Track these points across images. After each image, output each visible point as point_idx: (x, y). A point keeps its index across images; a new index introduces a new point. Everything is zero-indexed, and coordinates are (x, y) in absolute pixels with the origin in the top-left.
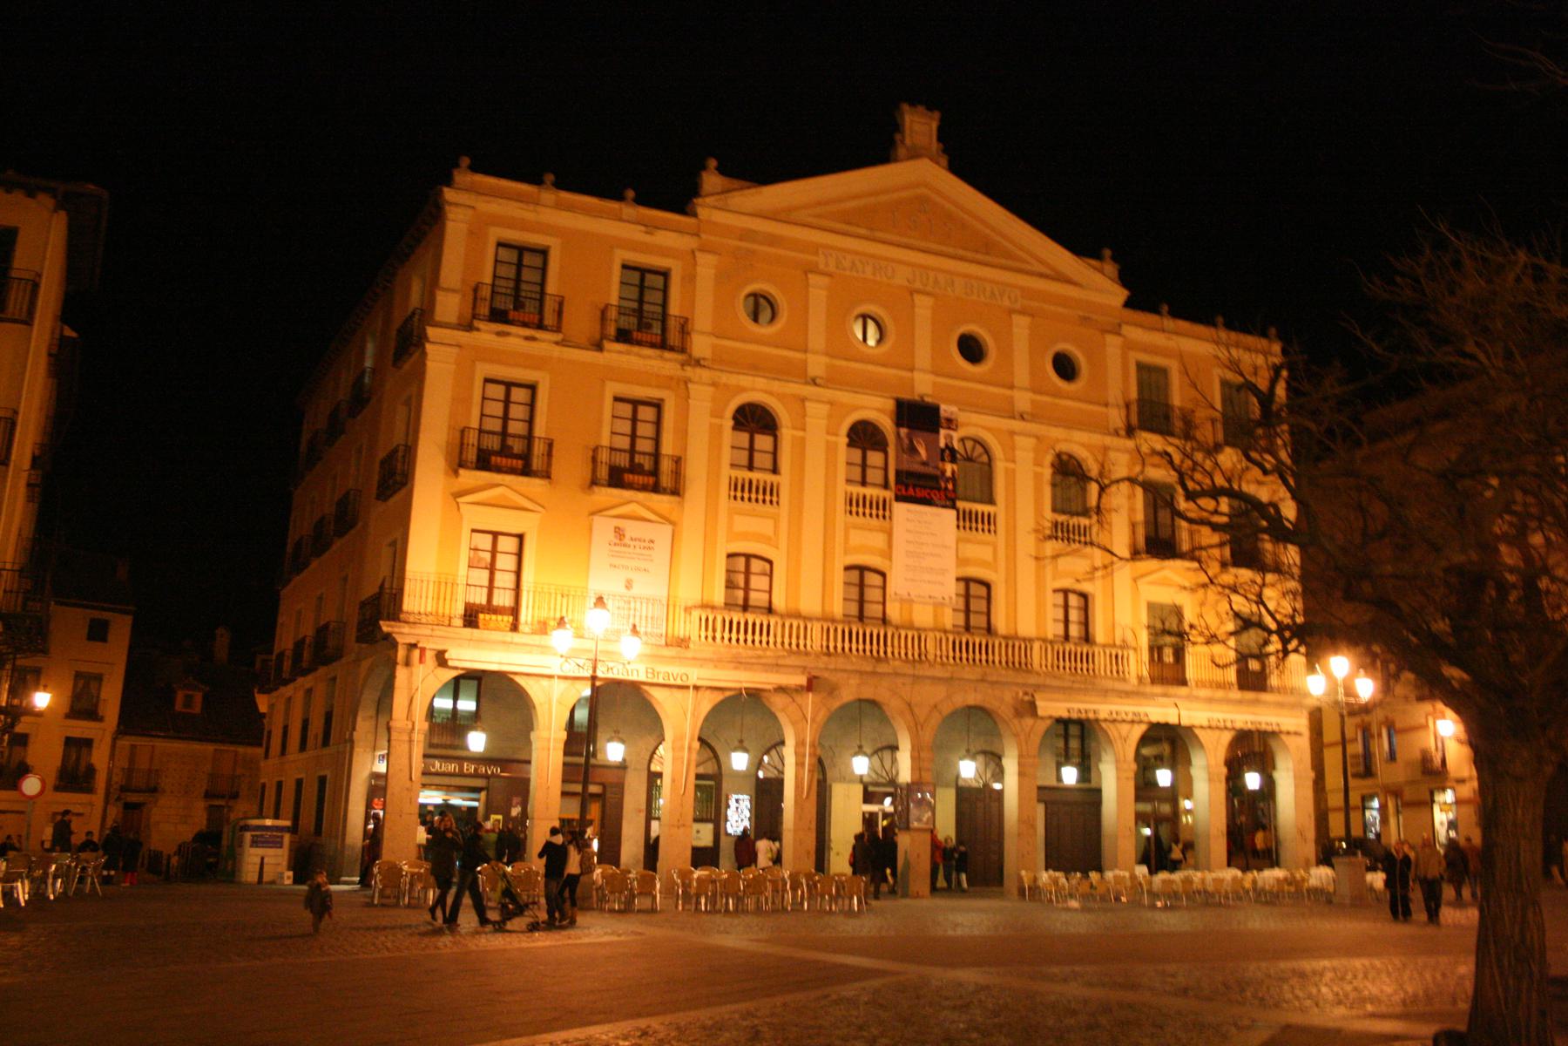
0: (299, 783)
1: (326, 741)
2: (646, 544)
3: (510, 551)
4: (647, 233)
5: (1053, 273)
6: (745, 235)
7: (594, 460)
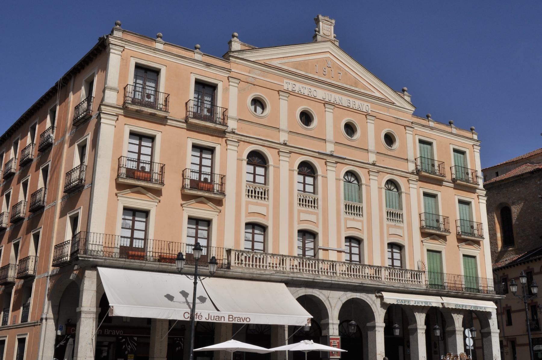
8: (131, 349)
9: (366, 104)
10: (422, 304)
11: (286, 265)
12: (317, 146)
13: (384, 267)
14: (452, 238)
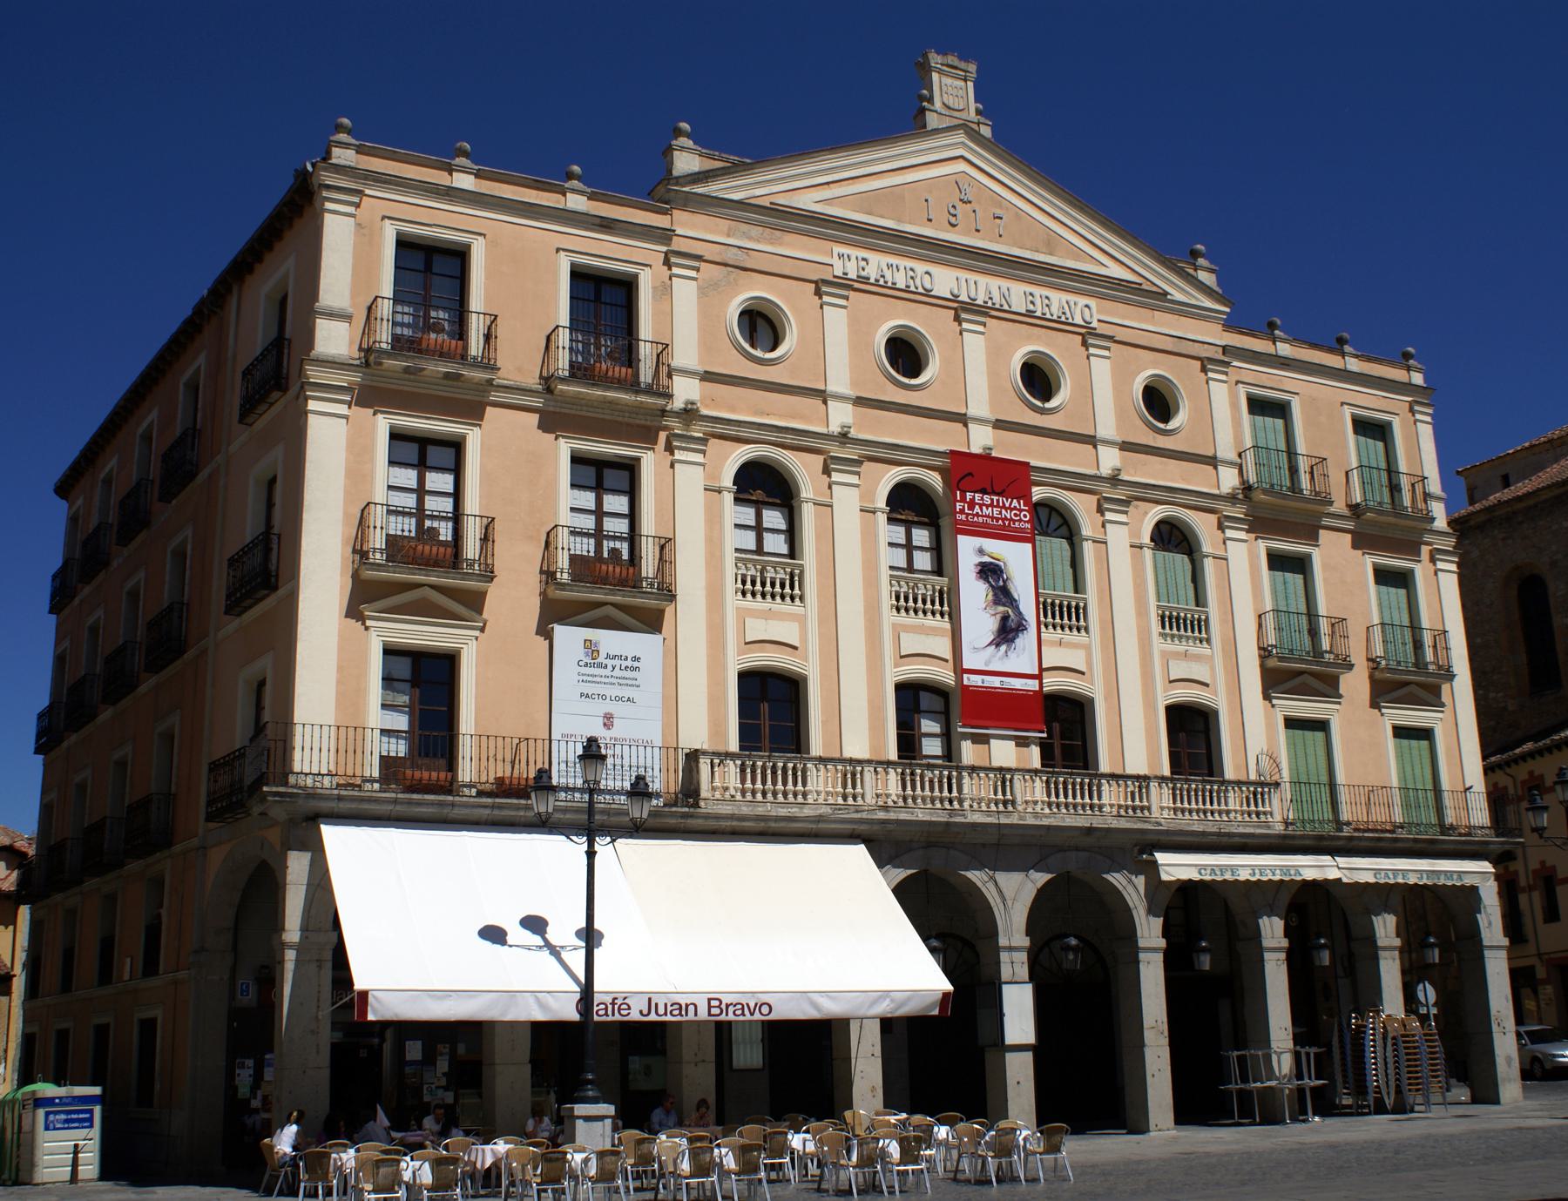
1: (150, 966)
2: (629, 663)
3: (938, 710)
9: (1083, 301)
10: (1274, 874)
11: (862, 787)
12: (943, 437)
13: (1156, 777)
14: (1355, 684)
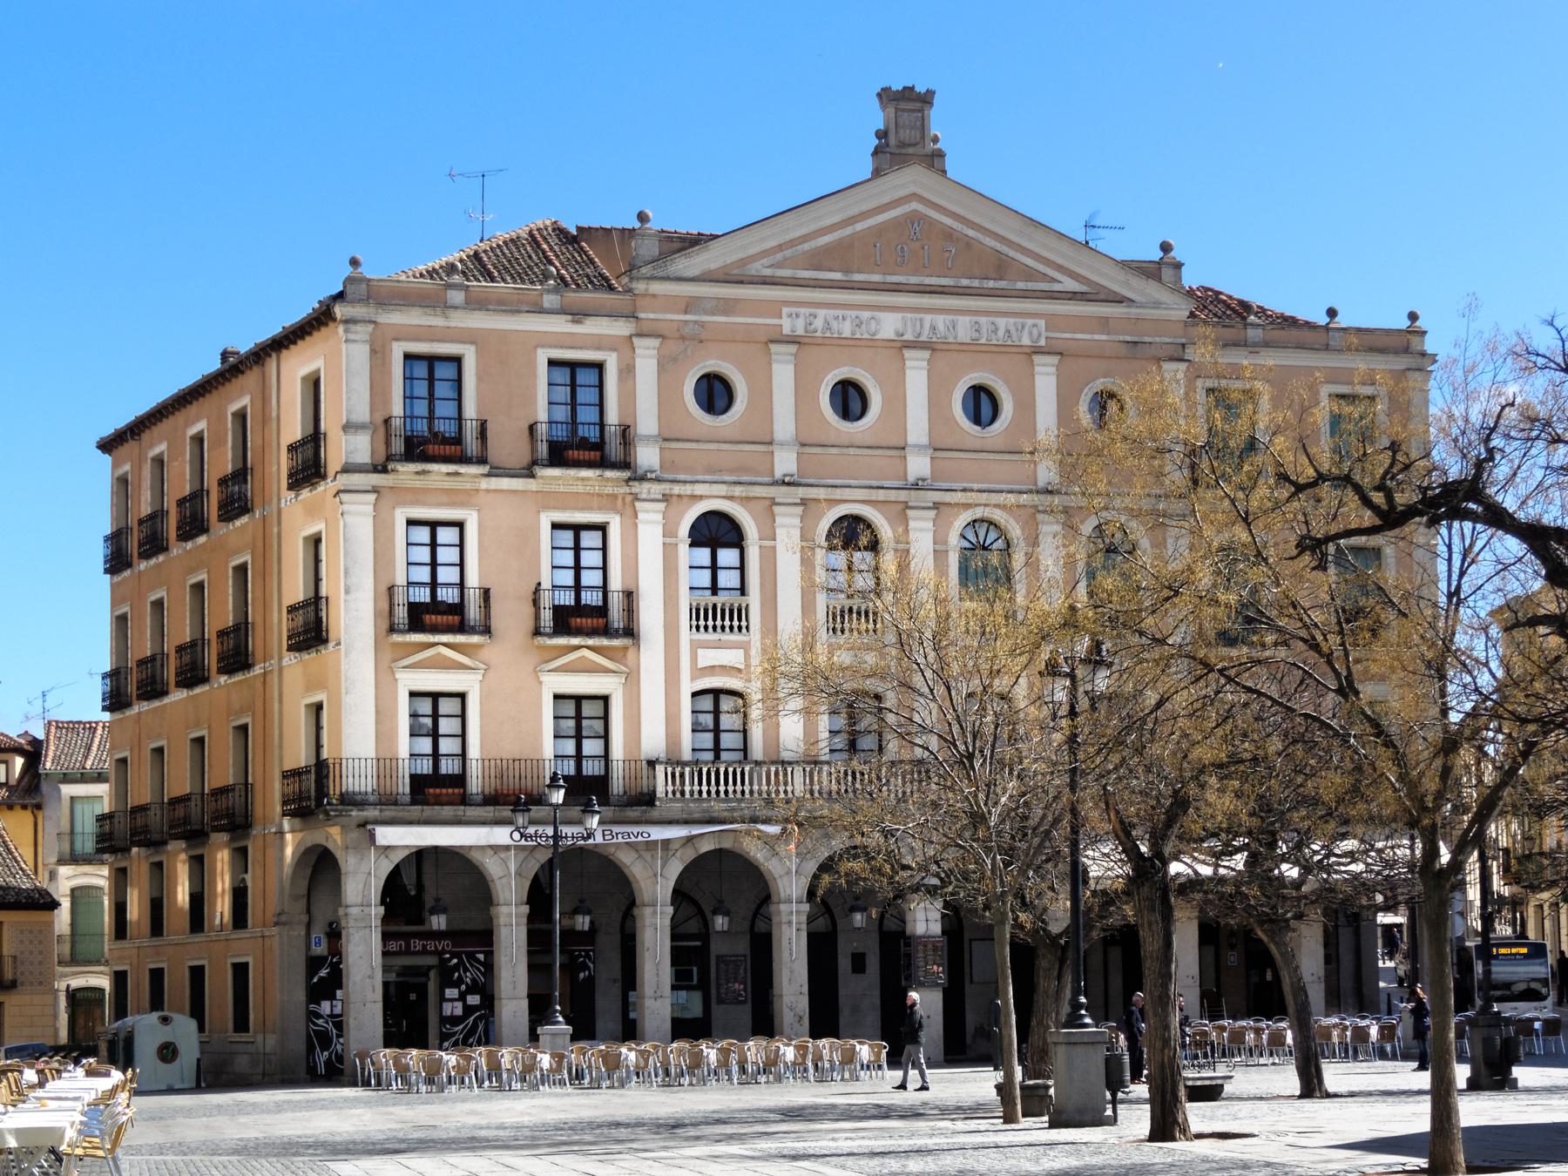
0: (197, 973)
4: (573, 321)
5: (1084, 288)
6: (690, 305)
7: (536, 602)
8: (473, 980)
